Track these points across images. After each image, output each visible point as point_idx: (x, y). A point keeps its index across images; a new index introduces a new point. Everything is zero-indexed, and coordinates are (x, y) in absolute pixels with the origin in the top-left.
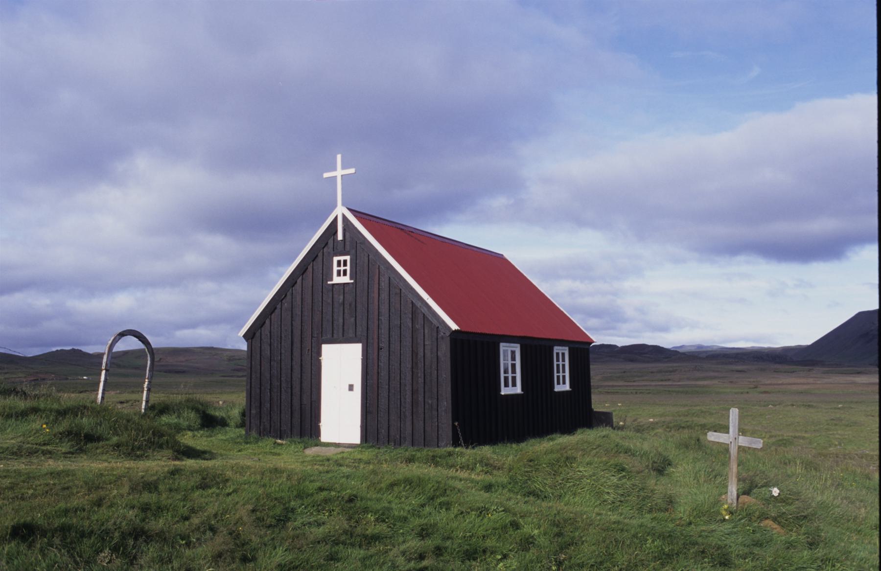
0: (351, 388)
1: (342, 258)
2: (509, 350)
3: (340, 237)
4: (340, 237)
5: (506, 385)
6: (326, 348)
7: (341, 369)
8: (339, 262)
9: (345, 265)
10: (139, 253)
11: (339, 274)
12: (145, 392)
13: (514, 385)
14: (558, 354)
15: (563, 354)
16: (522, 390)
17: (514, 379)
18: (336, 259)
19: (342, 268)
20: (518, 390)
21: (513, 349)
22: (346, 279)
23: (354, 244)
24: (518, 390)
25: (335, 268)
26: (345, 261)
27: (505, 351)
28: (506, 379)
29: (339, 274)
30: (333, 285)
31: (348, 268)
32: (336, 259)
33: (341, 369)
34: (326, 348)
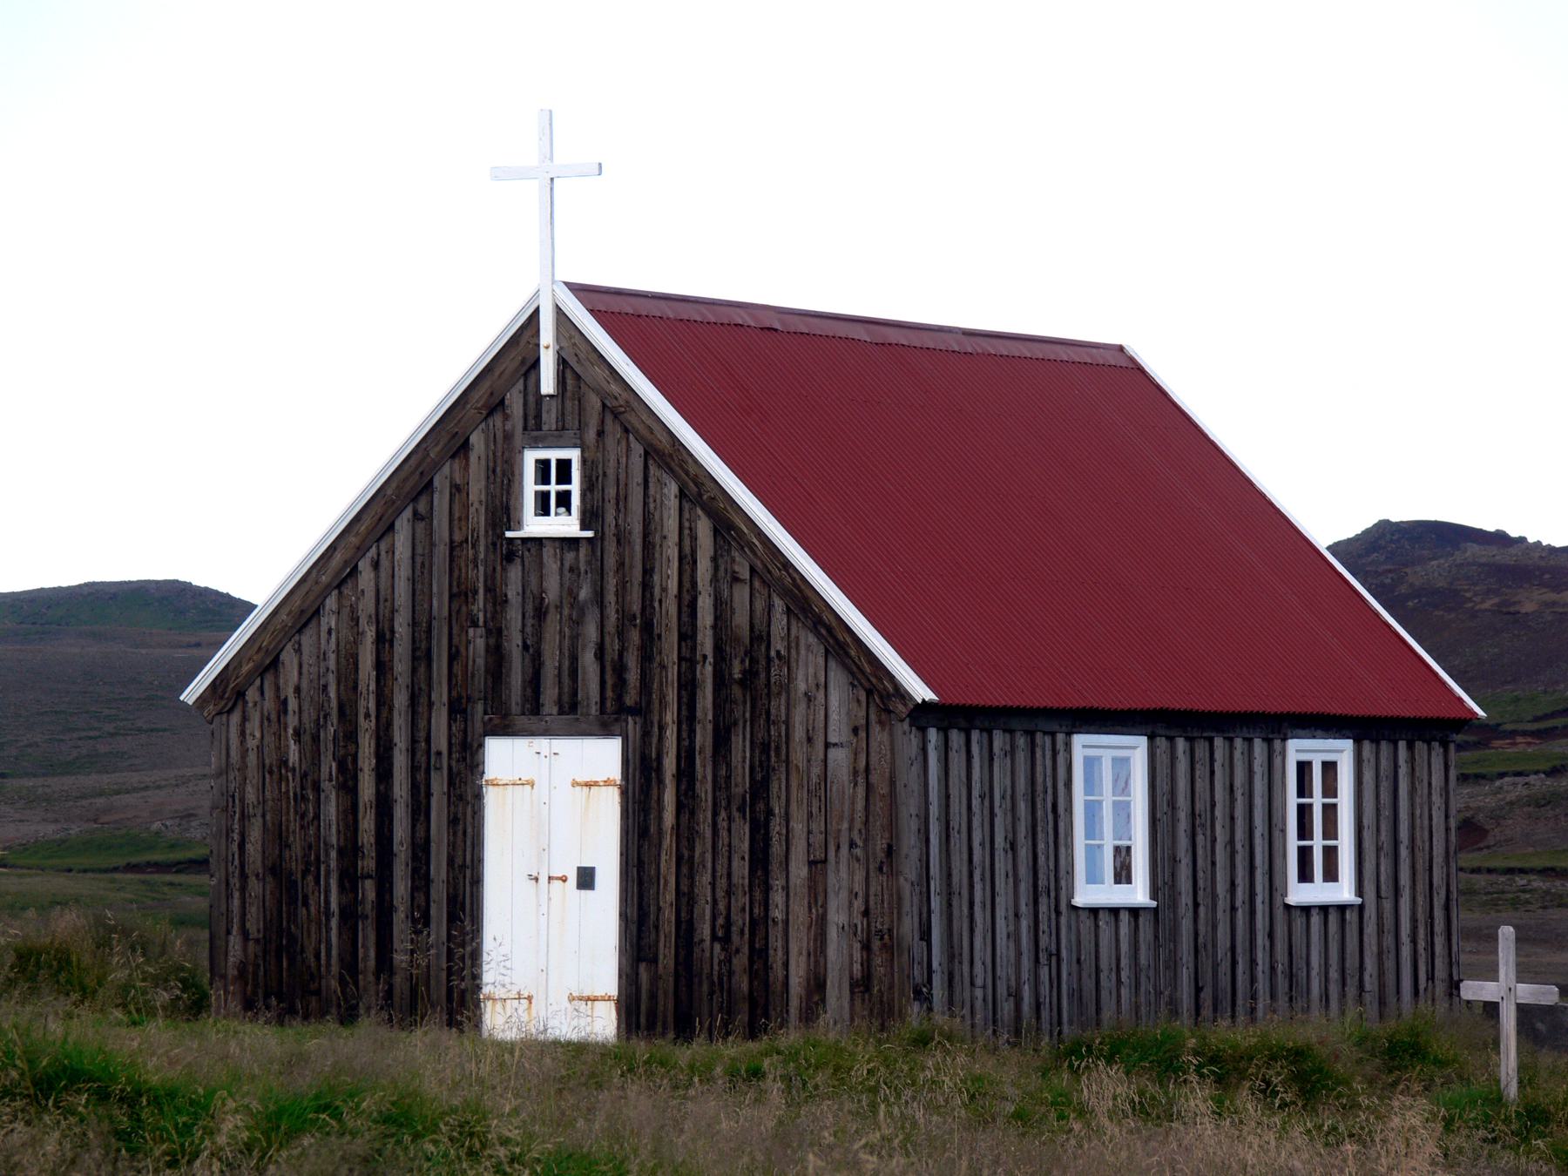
0: (586, 879)
1: (553, 455)
2: (1107, 757)
3: (548, 385)
4: (548, 385)
5: (1305, 875)
6: (503, 756)
7: (551, 821)
8: (543, 467)
9: (564, 477)
10: (209, 455)
11: (543, 508)
12: (334, 906)
13: (1331, 875)
14: (1304, 768)
15: (1330, 768)
16: (1154, 894)
17: (1331, 854)
18: (531, 457)
19: (553, 488)
20: (1138, 893)
21: (1329, 757)
22: (565, 525)
23: (589, 403)
24: (1344, 891)
25: (530, 487)
26: (564, 466)
27: (1090, 763)
28: (1305, 855)
29: (543, 508)
30: (525, 540)
31: (575, 487)
32: (531, 457)
33: (551, 821)
34: (503, 756)
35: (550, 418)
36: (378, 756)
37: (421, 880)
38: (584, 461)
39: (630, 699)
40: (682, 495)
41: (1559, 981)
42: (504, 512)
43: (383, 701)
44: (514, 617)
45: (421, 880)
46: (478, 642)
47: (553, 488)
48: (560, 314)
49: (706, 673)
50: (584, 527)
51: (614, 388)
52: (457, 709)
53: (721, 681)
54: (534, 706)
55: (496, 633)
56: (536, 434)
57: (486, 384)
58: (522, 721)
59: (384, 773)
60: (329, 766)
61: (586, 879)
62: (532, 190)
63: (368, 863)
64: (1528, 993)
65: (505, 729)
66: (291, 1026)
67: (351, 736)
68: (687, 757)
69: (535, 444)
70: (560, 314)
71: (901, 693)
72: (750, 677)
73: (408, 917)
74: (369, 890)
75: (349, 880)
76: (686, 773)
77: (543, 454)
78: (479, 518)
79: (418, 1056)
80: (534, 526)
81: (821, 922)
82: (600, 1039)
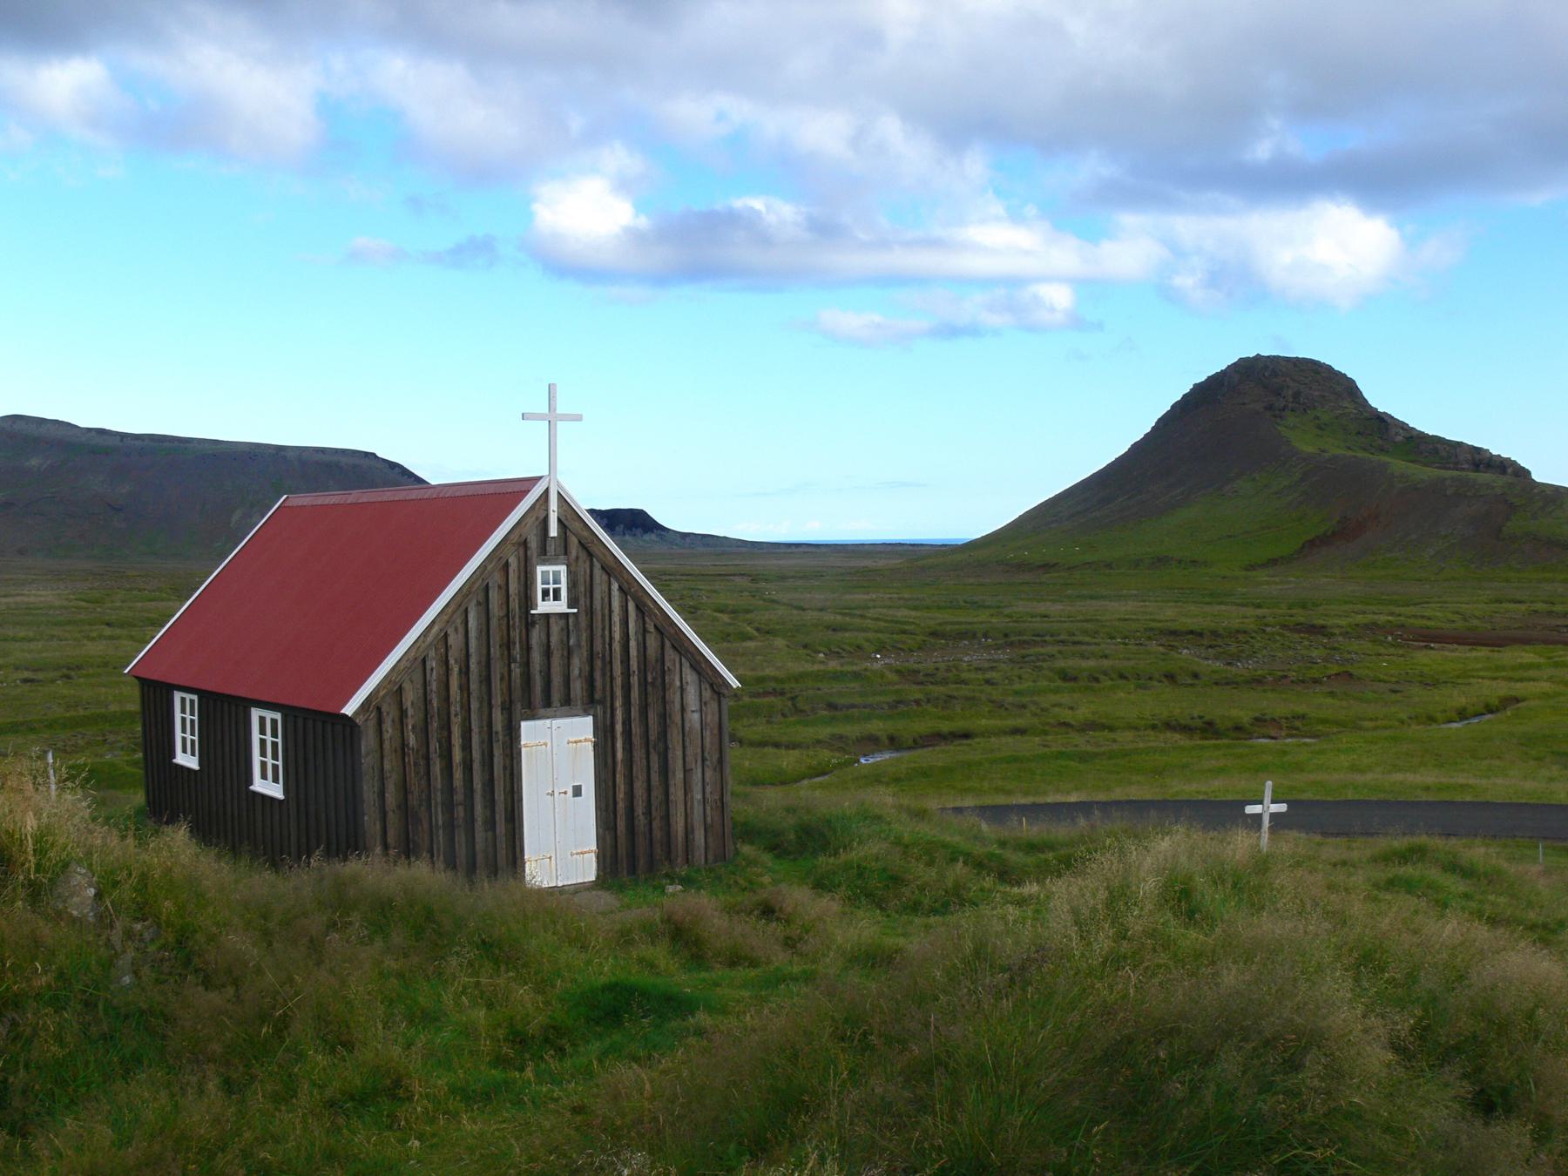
0: (577, 791)
3: (553, 531)
4: (553, 531)
6: (531, 732)
7: (558, 758)
9: (545, 593)
19: (551, 587)
33: (558, 758)
34: (531, 732)
35: (551, 548)
36: (463, 737)
37: (491, 803)
38: (569, 572)
39: (597, 696)
40: (620, 588)
41: (1289, 798)
42: (527, 600)
43: (467, 708)
44: (537, 657)
45: (491, 803)
46: (517, 670)
47: (551, 587)
48: (547, 491)
49: (635, 680)
50: (569, 607)
51: (586, 534)
52: (508, 708)
53: (644, 683)
54: (548, 704)
55: (527, 664)
56: (544, 556)
57: (517, 532)
58: (542, 711)
59: (467, 747)
60: (434, 745)
61: (577, 791)
62: (560, 410)
63: (459, 797)
64: (1275, 808)
65: (533, 717)
66: (219, 857)
67: (446, 726)
68: (627, 722)
69: (544, 563)
70: (547, 491)
71: (728, 685)
72: (654, 682)
73: (489, 819)
74: (460, 812)
75: (449, 807)
76: (628, 733)
77: (545, 568)
78: (515, 604)
79: (488, 893)
80: (543, 607)
81: (690, 807)
82: (214, 852)
